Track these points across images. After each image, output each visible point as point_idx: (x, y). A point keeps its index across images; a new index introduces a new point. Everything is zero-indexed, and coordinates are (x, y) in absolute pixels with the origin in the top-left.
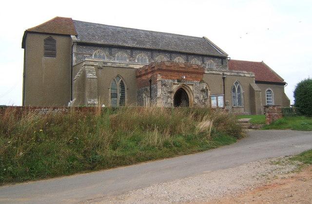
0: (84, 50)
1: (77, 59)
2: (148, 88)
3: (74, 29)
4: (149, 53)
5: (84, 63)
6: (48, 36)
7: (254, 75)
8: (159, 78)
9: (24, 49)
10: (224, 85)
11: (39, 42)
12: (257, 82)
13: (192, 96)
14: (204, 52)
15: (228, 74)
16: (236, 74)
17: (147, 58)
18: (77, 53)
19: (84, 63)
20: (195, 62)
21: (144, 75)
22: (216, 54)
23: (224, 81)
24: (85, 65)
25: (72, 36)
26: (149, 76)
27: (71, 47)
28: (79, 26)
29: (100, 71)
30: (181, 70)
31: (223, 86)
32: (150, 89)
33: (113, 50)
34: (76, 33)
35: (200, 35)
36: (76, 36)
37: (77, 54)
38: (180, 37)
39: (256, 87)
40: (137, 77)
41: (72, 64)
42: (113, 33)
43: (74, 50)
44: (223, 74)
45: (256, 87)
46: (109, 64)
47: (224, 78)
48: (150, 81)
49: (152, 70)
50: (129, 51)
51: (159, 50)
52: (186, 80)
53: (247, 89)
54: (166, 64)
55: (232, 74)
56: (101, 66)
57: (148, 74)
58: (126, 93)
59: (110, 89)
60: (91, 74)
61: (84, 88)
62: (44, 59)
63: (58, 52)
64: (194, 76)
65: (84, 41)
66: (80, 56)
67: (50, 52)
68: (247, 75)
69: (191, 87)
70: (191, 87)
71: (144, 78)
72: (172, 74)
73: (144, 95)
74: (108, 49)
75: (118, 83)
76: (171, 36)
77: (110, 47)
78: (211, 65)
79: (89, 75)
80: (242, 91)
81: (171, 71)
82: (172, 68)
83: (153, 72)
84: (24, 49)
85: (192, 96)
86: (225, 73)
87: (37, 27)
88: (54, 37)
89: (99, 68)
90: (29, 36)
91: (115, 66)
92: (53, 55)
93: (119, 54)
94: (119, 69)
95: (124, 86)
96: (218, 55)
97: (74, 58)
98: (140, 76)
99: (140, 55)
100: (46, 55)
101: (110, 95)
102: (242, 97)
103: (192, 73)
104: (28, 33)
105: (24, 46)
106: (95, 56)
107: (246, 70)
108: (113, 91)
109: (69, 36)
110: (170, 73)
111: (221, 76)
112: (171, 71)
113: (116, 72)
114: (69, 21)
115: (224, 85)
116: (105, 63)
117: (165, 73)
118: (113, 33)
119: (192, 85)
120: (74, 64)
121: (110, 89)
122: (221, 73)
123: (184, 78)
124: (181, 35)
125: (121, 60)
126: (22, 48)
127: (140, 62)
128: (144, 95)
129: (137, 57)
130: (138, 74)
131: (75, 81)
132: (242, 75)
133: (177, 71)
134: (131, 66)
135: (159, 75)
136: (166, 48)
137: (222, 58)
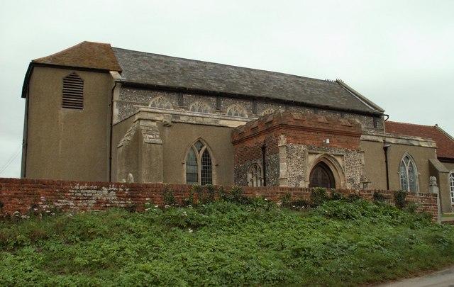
0: (134, 95)
1: (122, 111)
2: (259, 163)
3: (115, 61)
4: (249, 104)
5: (137, 117)
6: (71, 72)
7: (434, 145)
8: (283, 141)
9: (24, 100)
10: (386, 162)
11: (53, 85)
12: (442, 159)
13: (342, 178)
14: (344, 105)
15: (393, 141)
16: (405, 142)
17: (245, 112)
18: (120, 102)
19: (137, 117)
20: (345, 120)
21: (250, 138)
22: (358, 108)
23: (386, 154)
24: (139, 119)
25: (111, 72)
26: (261, 139)
27: (110, 92)
28: (122, 58)
29: (167, 130)
30: (321, 127)
31: (385, 165)
32: (264, 164)
33: (185, 96)
34: (119, 67)
35: (333, 79)
36: (120, 72)
37: (121, 104)
38: (298, 80)
39: (440, 166)
40: (235, 143)
41: (112, 121)
42: (181, 69)
43: (117, 96)
44: (385, 142)
45: (440, 166)
46: (183, 119)
47: (385, 149)
48: (264, 148)
49: (269, 127)
50: (213, 99)
51: (267, 98)
52: (330, 147)
53: (425, 169)
54: (295, 117)
55: (400, 141)
56: (169, 121)
57: (259, 134)
58: (214, 173)
59: (185, 166)
60: (152, 137)
61: (138, 162)
62: (63, 112)
63: (86, 102)
64: (343, 139)
65: (134, 80)
66: (126, 107)
67: (73, 99)
68: (424, 144)
69: (339, 160)
70: (339, 160)
71: (251, 144)
72: (306, 134)
73: (250, 176)
74: (175, 95)
75: (200, 156)
76: (283, 78)
77: (180, 91)
78: (363, 123)
79: (148, 138)
80: (417, 173)
81: (304, 129)
82: (306, 124)
83: (268, 130)
84: (24, 100)
85: (342, 178)
86: (387, 140)
87: (51, 56)
88: (81, 75)
89: (165, 125)
90: (37, 72)
91: (195, 123)
92: (78, 105)
93: (197, 103)
94: (202, 128)
95: (210, 160)
96: (362, 109)
97: (116, 111)
98: (241, 141)
99: (232, 107)
100: (66, 104)
101: (185, 175)
102: (417, 183)
103: (341, 133)
104: (34, 65)
105: (26, 92)
106: (154, 105)
107: (422, 137)
108: (192, 169)
109: (107, 72)
110: (302, 132)
111: (380, 146)
112: (304, 129)
113: (195, 134)
114: (107, 49)
115: (386, 162)
116: (175, 116)
117: (292, 133)
118: (181, 69)
119: (342, 156)
120: (115, 121)
121: (185, 166)
122: (381, 140)
123: (328, 142)
124: (300, 77)
125: (200, 112)
126: (23, 96)
127: (237, 118)
128: (250, 176)
129: (228, 111)
130: (238, 138)
131: (121, 148)
132: (416, 143)
133: (316, 130)
134: (222, 122)
135: (282, 136)
136: (278, 96)
137: (376, 115)
